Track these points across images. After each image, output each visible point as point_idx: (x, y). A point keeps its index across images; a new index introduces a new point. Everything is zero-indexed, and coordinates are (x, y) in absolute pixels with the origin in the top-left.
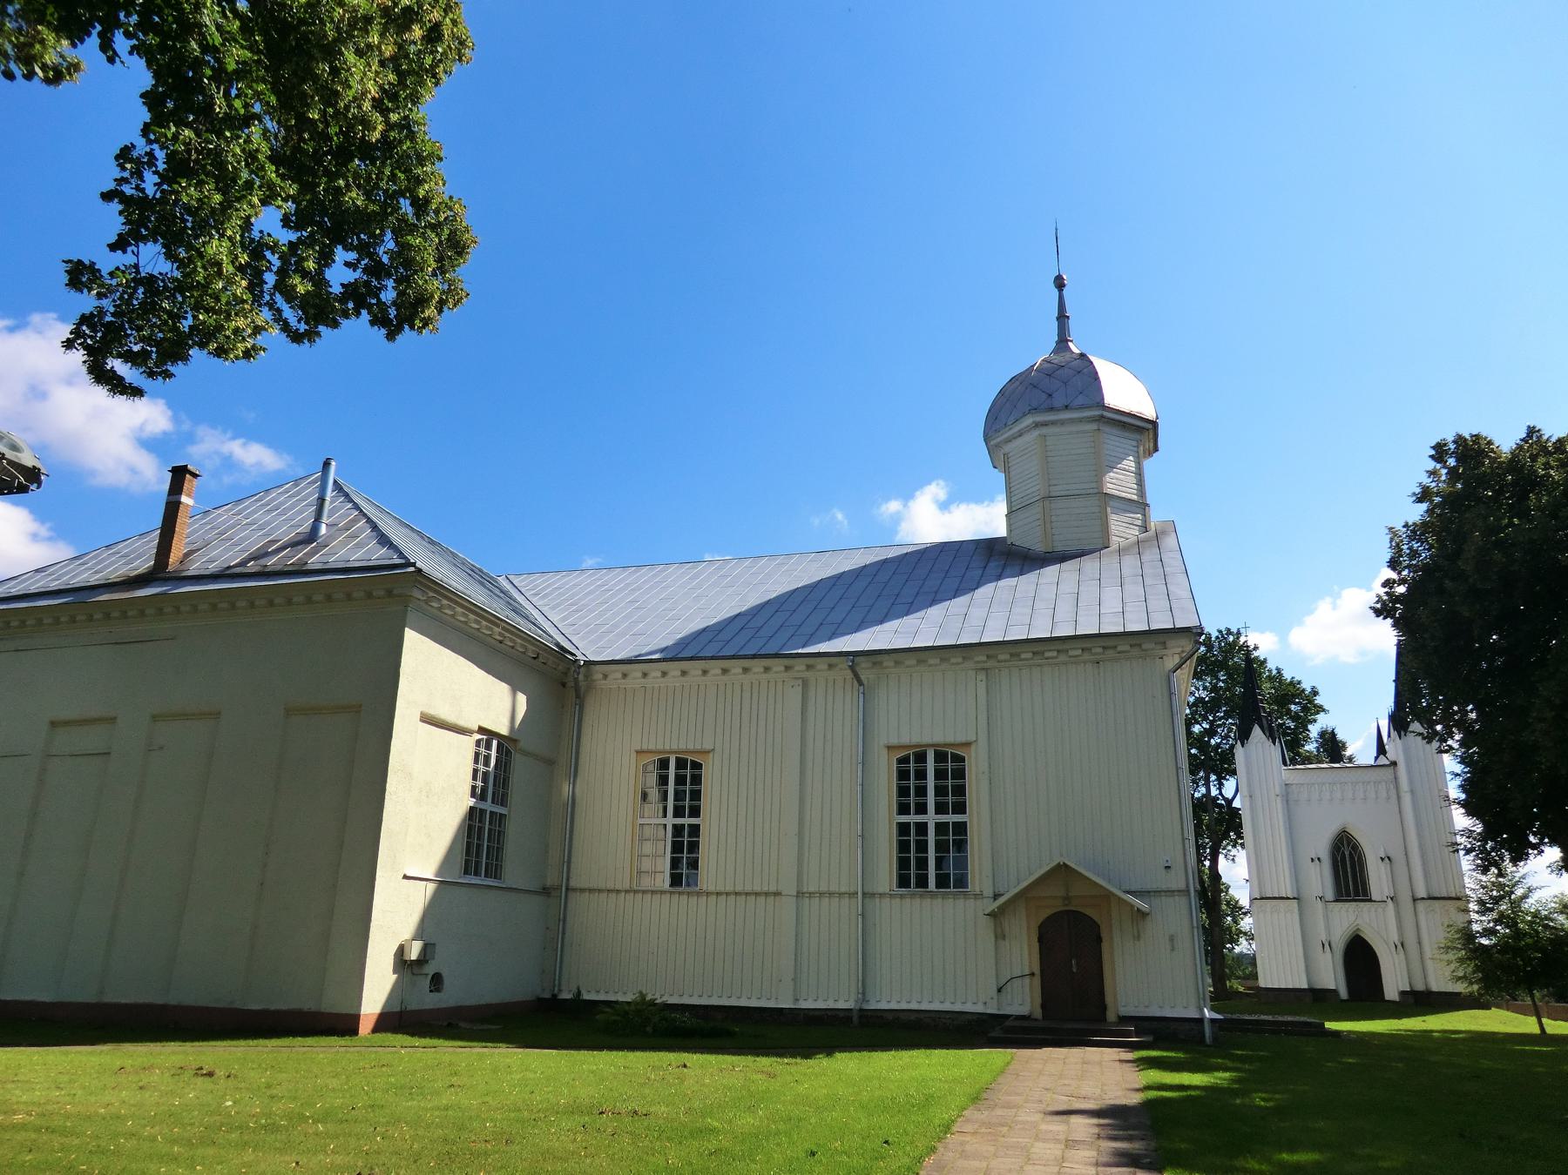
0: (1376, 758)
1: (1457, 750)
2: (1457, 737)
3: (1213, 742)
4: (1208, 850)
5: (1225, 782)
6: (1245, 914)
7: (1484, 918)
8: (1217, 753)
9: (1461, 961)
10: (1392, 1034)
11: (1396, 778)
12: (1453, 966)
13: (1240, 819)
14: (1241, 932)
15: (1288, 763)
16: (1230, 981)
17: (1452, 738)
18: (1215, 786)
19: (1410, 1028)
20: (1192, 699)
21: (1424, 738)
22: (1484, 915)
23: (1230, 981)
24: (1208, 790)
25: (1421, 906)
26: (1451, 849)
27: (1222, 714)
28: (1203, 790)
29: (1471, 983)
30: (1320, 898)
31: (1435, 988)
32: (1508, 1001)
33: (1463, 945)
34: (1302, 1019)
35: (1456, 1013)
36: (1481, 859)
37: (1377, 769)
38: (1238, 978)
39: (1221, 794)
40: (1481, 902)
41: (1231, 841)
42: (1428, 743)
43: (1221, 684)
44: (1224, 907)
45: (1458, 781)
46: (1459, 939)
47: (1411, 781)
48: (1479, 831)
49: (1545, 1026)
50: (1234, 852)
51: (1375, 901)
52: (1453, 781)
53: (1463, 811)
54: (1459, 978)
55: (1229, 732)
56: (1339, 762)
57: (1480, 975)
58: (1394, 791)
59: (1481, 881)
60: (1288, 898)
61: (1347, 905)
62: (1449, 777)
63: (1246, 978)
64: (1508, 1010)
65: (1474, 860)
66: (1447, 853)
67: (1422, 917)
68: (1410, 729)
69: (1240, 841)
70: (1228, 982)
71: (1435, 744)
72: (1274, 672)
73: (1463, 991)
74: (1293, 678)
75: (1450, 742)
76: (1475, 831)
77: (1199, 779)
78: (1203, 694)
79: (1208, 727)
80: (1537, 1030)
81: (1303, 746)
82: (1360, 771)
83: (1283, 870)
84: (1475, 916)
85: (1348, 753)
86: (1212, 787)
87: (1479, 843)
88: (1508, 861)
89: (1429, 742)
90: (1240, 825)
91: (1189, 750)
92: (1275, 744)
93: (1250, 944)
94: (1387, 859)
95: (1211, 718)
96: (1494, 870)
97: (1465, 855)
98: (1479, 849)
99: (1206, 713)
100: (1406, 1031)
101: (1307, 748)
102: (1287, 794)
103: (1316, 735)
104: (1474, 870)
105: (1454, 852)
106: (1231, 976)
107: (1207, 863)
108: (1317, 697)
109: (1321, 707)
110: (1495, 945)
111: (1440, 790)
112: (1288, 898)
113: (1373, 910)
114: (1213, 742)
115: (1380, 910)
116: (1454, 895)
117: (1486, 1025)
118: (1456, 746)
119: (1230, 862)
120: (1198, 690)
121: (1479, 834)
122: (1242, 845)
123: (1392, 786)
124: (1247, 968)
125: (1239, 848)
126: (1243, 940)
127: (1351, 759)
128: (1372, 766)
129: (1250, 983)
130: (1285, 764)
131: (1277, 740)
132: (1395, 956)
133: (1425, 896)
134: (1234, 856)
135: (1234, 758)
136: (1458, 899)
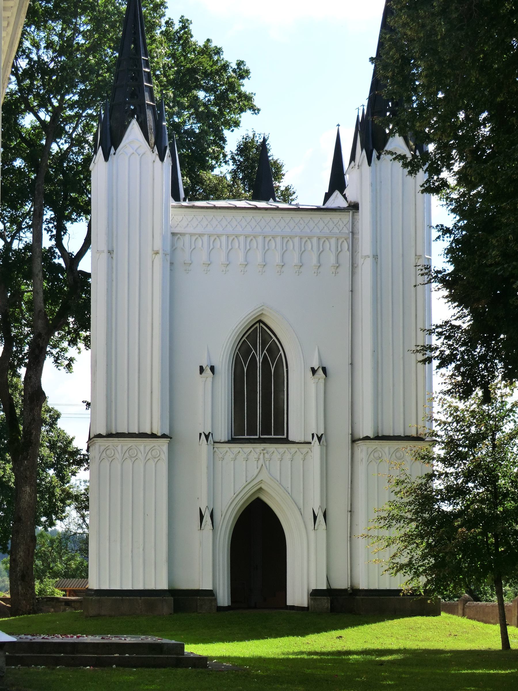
0: (327, 196)
1: (454, 189)
2: (456, 167)
3: (54, 148)
4: (27, 348)
5: (68, 225)
6: (79, 463)
7: (451, 470)
8: (59, 169)
9: (408, 538)
10: (288, 659)
11: (353, 233)
12: (394, 548)
13: (88, 292)
14: (68, 495)
15: (182, 195)
16: (42, 582)
17: (449, 167)
18: (49, 230)
19: (318, 650)
20: (23, 63)
21: (405, 165)
22: (452, 465)
23: (42, 582)
24: (38, 238)
25: (362, 448)
26: (420, 357)
27: (76, 98)
28: (28, 237)
29: (417, 574)
30: (207, 437)
31: (363, 585)
32: (466, 601)
33: (416, 513)
34: (150, 639)
35: (388, 623)
36: (463, 374)
37: (327, 217)
38: (55, 575)
39: (59, 244)
40: (451, 444)
41: (69, 333)
42: (410, 173)
43: (80, 40)
44: (45, 451)
45: (446, 242)
46: (410, 503)
47: (376, 240)
48: (465, 326)
49: (511, 639)
50: (72, 352)
51: (293, 443)
52: (439, 242)
53: (446, 292)
54: (402, 567)
55: (84, 132)
56: (267, 199)
57: (433, 561)
58: (348, 254)
59: (456, 409)
60: (153, 436)
61: (248, 448)
62: (435, 233)
63: (68, 575)
64: (463, 615)
65: (452, 376)
66: (413, 362)
67: (361, 469)
68: (388, 147)
69: (83, 334)
70: (37, 583)
71: (422, 176)
72: (177, 26)
73: (404, 587)
74: (208, 40)
75: (445, 174)
76: (459, 327)
77: (24, 216)
78: (46, 56)
79: (48, 119)
80: (497, 645)
81: (212, 168)
82: (297, 216)
83: (221, 403)
84: (439, 467)
85: (282, 185)
86: (44, 232)
87: (463, 349)
88: (500, 378)
89: (413, 172)
90: (87, 305)
91: (7, 160)
92: (162, 159)
93: (83, 517)
94: (320, 371)
95: (56, 103)
96: (479, 392)
97: (439, 367)
98: (462, 358)
99: (49, 92)
100: (310, 653)
101: (217, 171)
102: (174, 250)
103: (234, 149)
104: (448, 392)
105: (424, 361)
106: (44, 572)
107: (22, 371)
108: (245, 81)
109: (248, 98)
110: (461, 513)
111: (418, 257)
112: (153, 436)
113: (288, 456)
114: (54, 148)
115: (299, 457)
116: (414, 434)
117: (427, 639)
118: (452, 181)
119: (63, 370)
120: (38, 48)
121: (466, 331)
122: (87, 340)
123: (345, 245)
124: (73, 558)
125: (81, 345)
126: (71, 511)
127: (287, 195)
128: (319, 209)
129: (74, 584)
130: (176, 196)
131: (168, 151)
132: (312, 533)
133: (371, 435)
134: (71, 360)
135: (89, 182)
136: (419, 438)
